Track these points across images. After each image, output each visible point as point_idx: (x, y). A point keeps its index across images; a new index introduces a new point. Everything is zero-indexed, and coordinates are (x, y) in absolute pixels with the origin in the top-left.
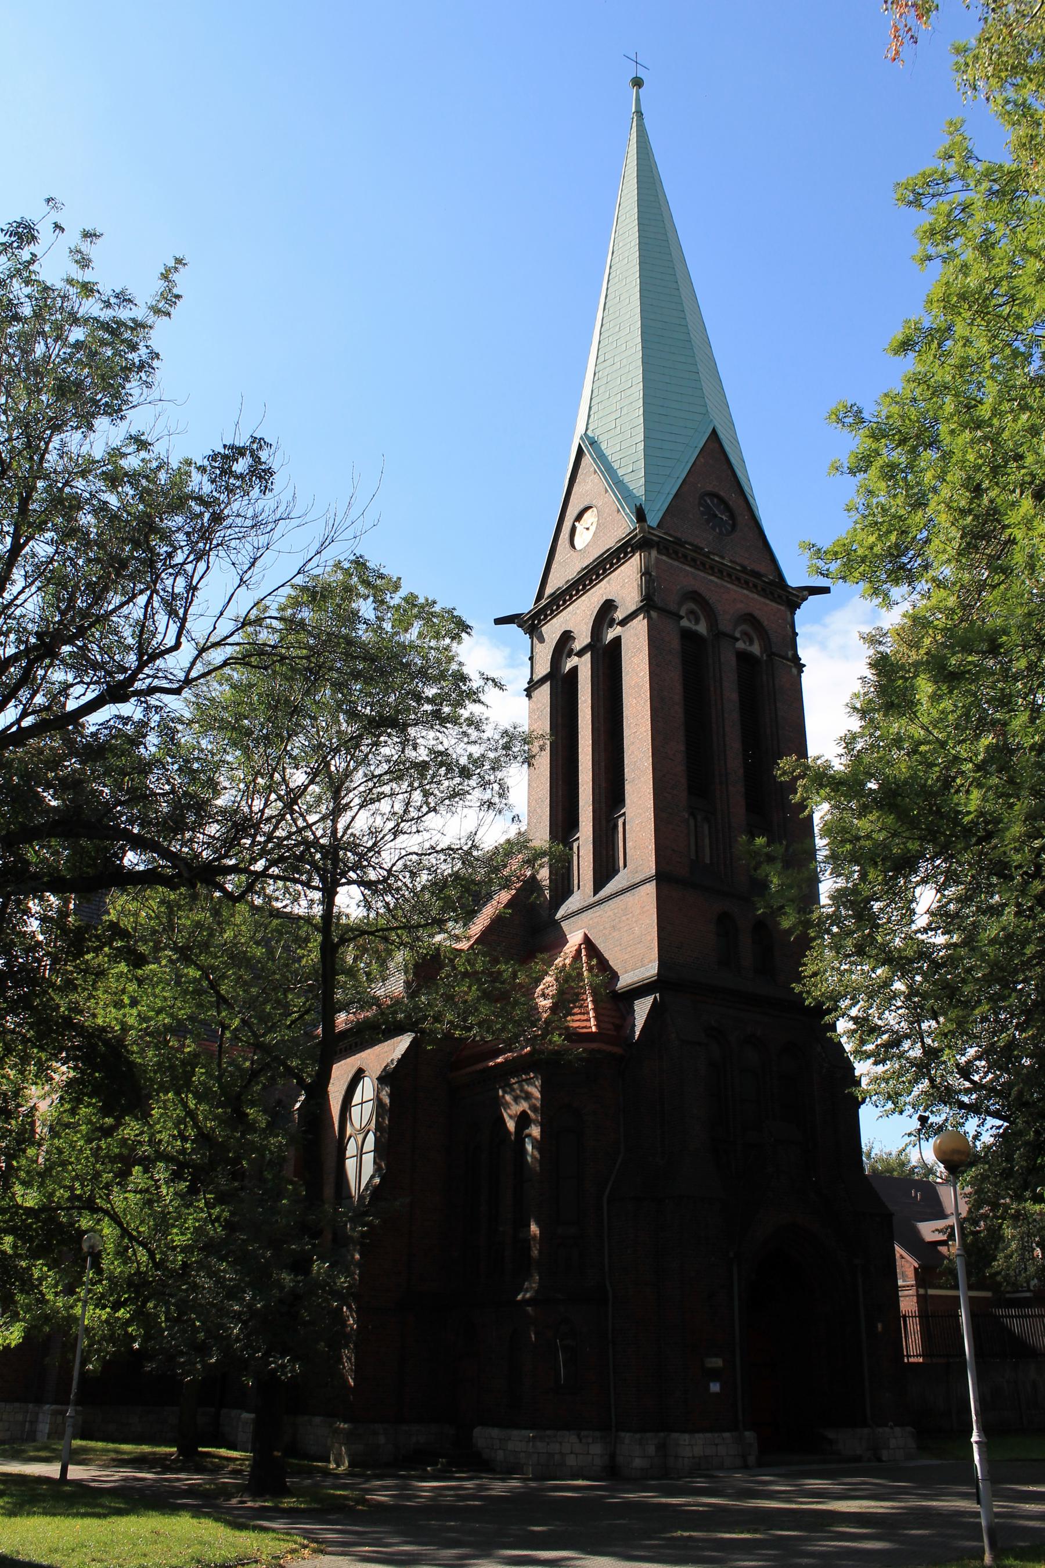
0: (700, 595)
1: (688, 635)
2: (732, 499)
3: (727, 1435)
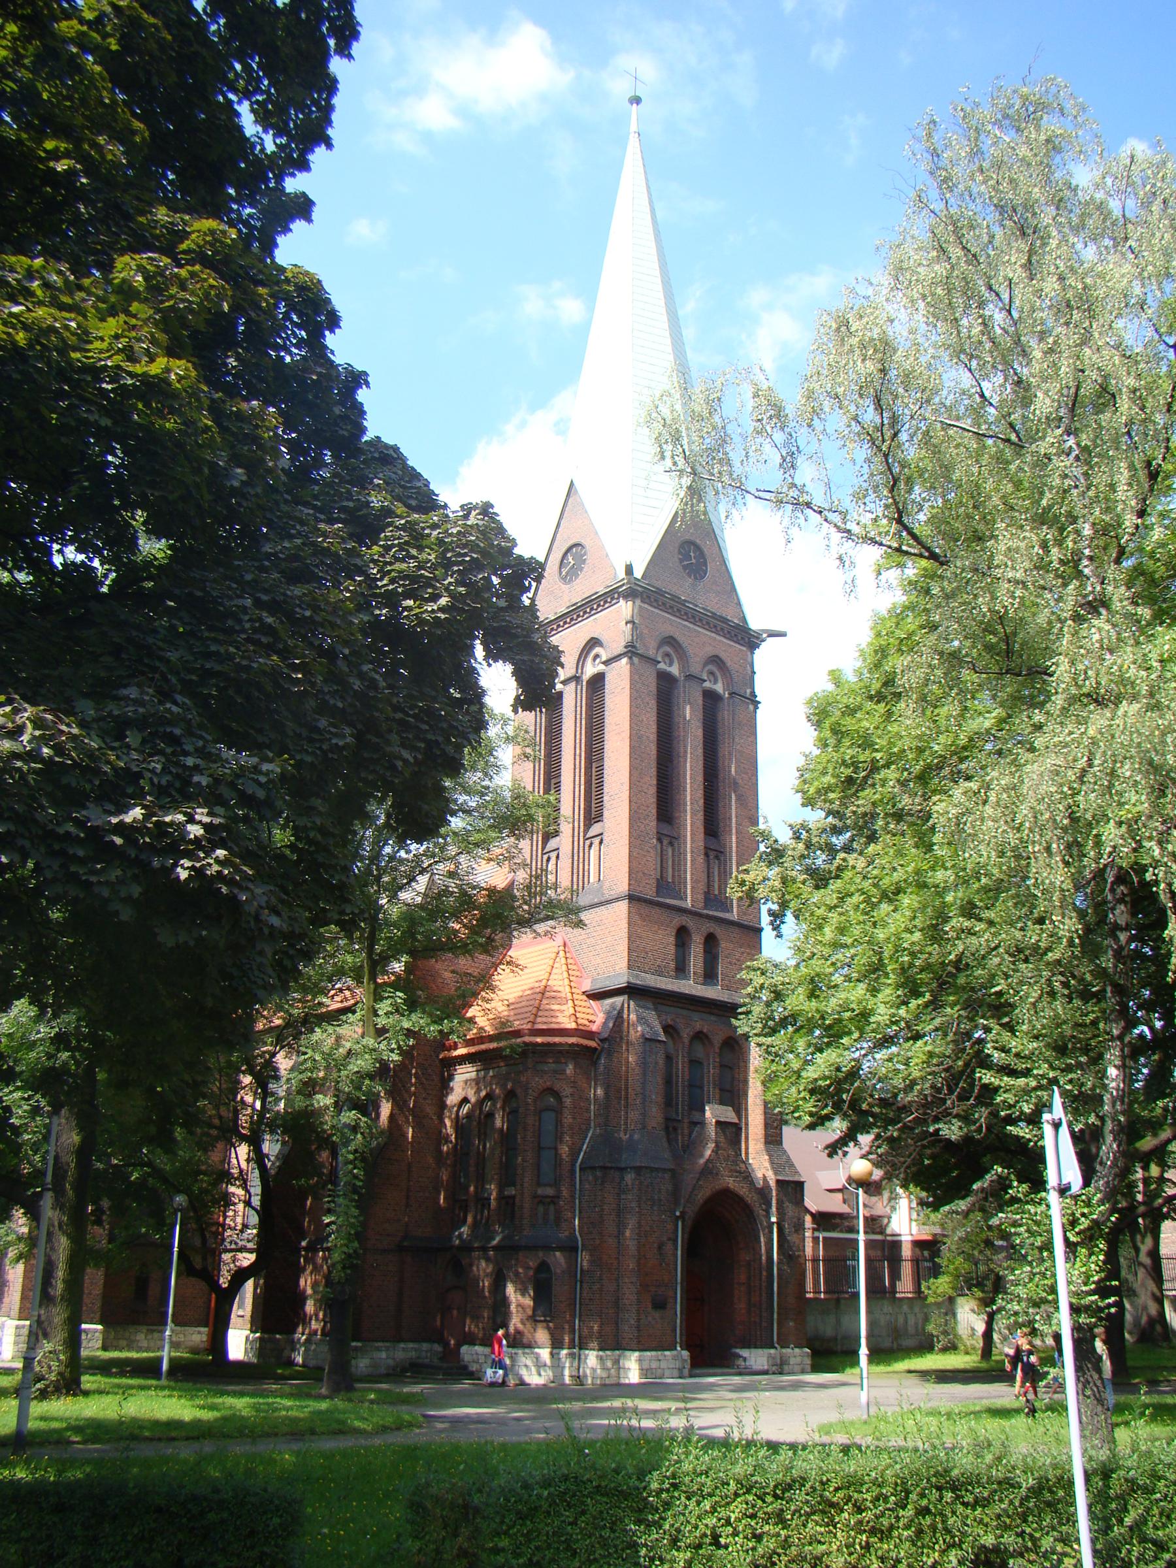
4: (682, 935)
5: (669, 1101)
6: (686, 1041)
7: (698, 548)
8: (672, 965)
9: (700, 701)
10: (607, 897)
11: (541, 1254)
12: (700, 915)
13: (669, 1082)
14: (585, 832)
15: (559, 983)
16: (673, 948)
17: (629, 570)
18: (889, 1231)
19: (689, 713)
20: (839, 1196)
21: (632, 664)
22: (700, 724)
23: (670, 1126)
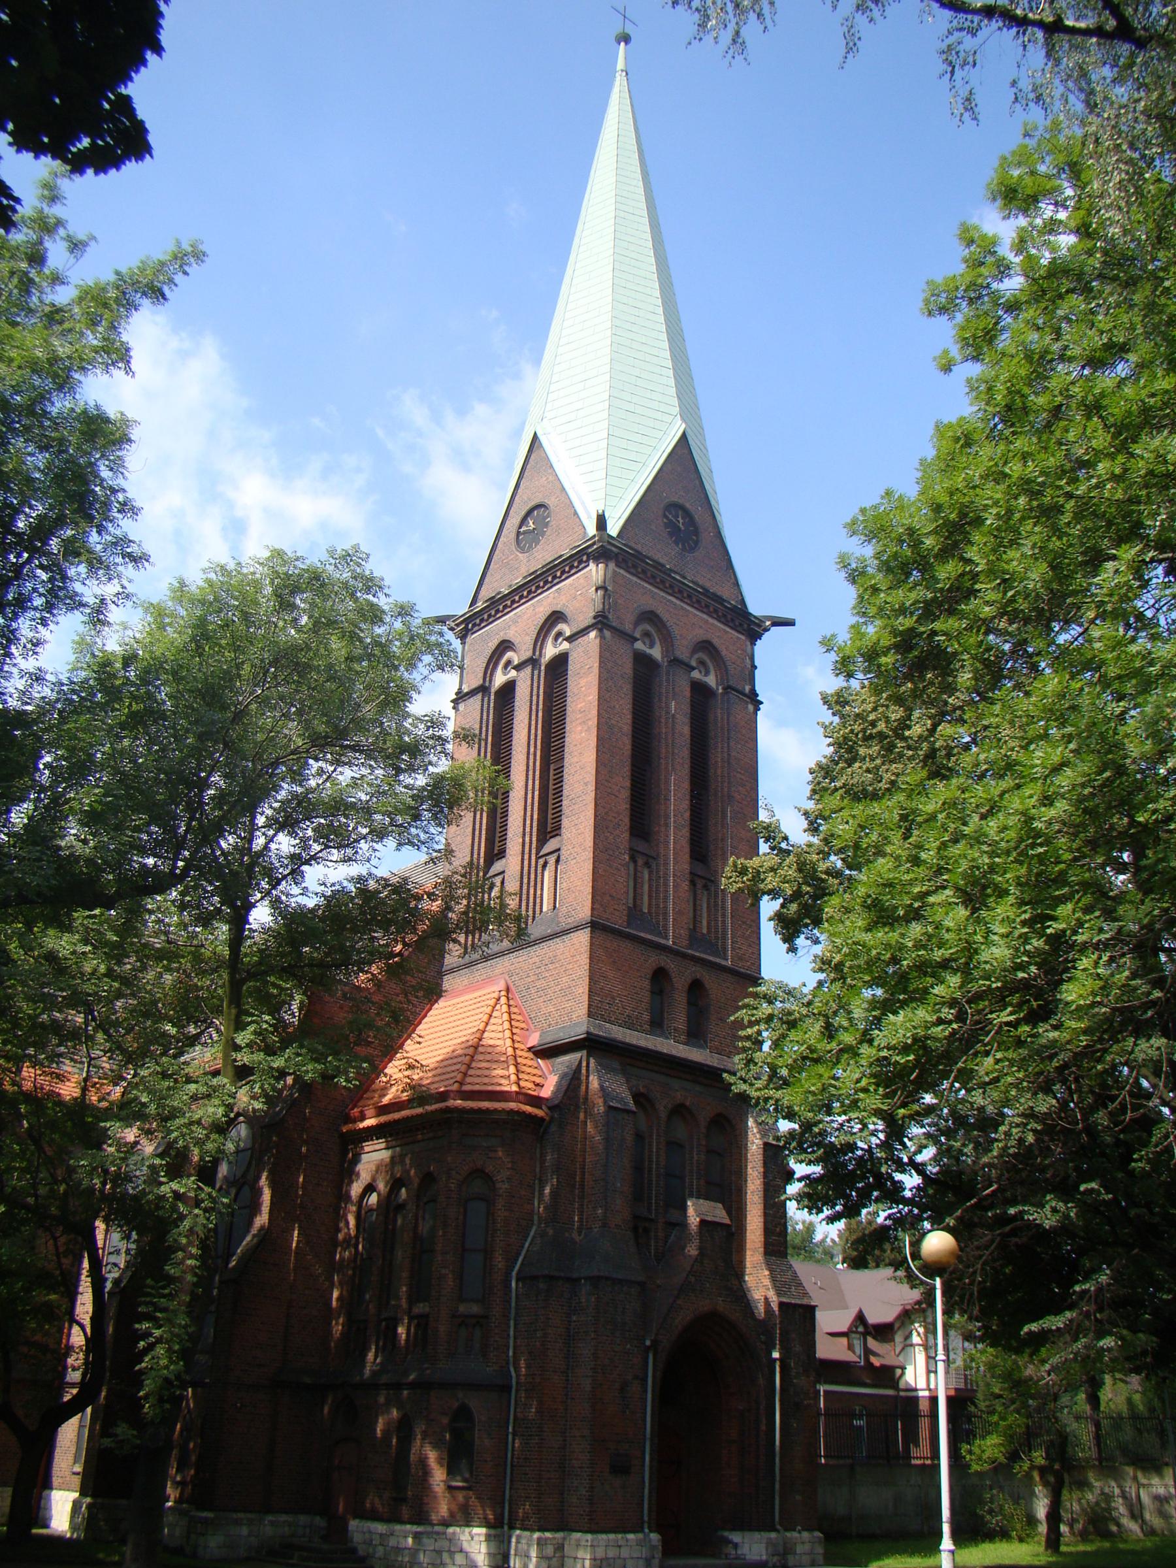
0: (657, 616)
1: (642, 660)
2: (698, 513)
3: (631, 1536)
4: (660, 976)
5: (639, 1194)
6: (663, 1115)
7: (687, 513)
8: (646, 1016)
9: (688, 693)
10: (564, 925)
11: (460, 1395)
12: (684, 956)
13: (639, 1168)
14: (539, 849)
15: (498, 1038)
16: (647, 994)
17: (601, 522)
18: (902, 1385)
19: (675, 711)
20: (844, 1340)
21: (602, 637)
22: (687, 721)
23: (640, 1227)
